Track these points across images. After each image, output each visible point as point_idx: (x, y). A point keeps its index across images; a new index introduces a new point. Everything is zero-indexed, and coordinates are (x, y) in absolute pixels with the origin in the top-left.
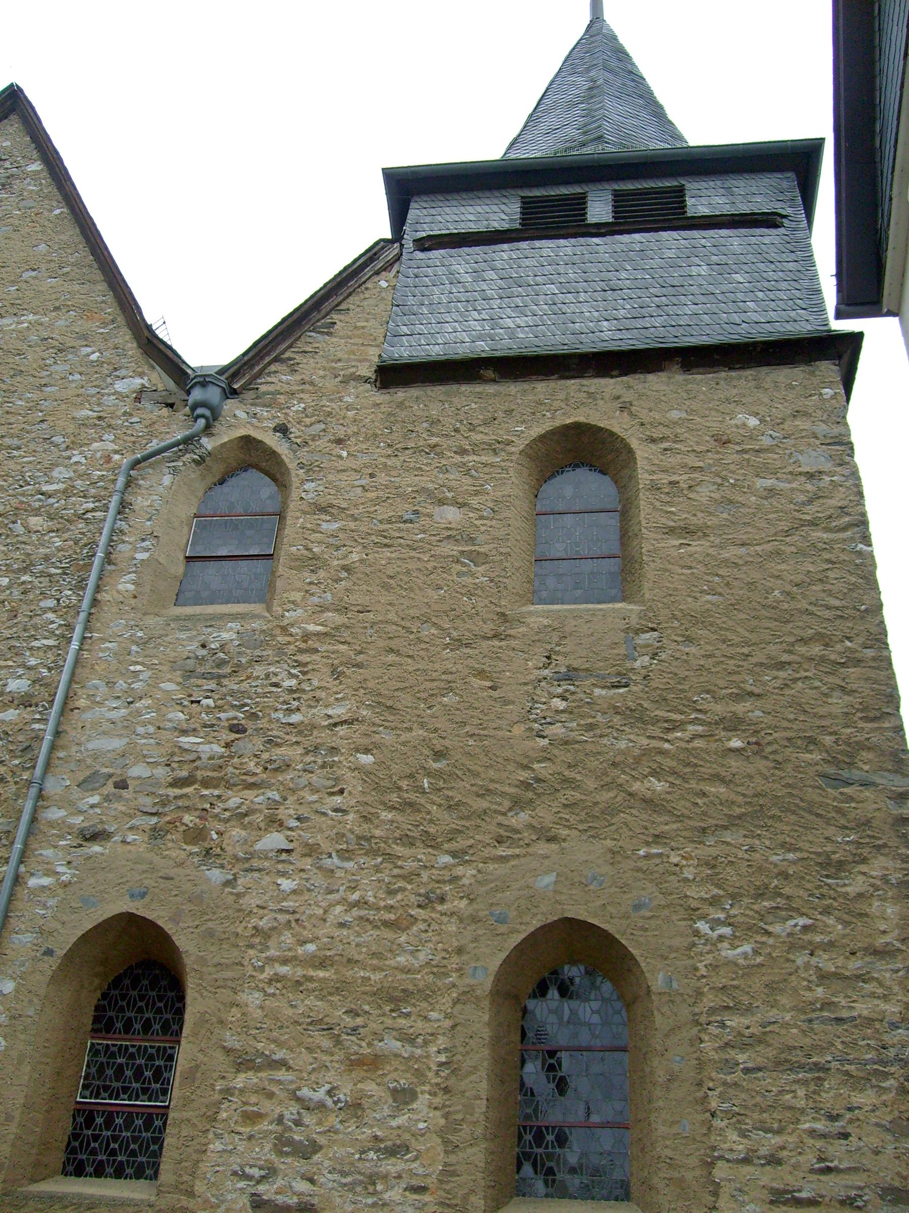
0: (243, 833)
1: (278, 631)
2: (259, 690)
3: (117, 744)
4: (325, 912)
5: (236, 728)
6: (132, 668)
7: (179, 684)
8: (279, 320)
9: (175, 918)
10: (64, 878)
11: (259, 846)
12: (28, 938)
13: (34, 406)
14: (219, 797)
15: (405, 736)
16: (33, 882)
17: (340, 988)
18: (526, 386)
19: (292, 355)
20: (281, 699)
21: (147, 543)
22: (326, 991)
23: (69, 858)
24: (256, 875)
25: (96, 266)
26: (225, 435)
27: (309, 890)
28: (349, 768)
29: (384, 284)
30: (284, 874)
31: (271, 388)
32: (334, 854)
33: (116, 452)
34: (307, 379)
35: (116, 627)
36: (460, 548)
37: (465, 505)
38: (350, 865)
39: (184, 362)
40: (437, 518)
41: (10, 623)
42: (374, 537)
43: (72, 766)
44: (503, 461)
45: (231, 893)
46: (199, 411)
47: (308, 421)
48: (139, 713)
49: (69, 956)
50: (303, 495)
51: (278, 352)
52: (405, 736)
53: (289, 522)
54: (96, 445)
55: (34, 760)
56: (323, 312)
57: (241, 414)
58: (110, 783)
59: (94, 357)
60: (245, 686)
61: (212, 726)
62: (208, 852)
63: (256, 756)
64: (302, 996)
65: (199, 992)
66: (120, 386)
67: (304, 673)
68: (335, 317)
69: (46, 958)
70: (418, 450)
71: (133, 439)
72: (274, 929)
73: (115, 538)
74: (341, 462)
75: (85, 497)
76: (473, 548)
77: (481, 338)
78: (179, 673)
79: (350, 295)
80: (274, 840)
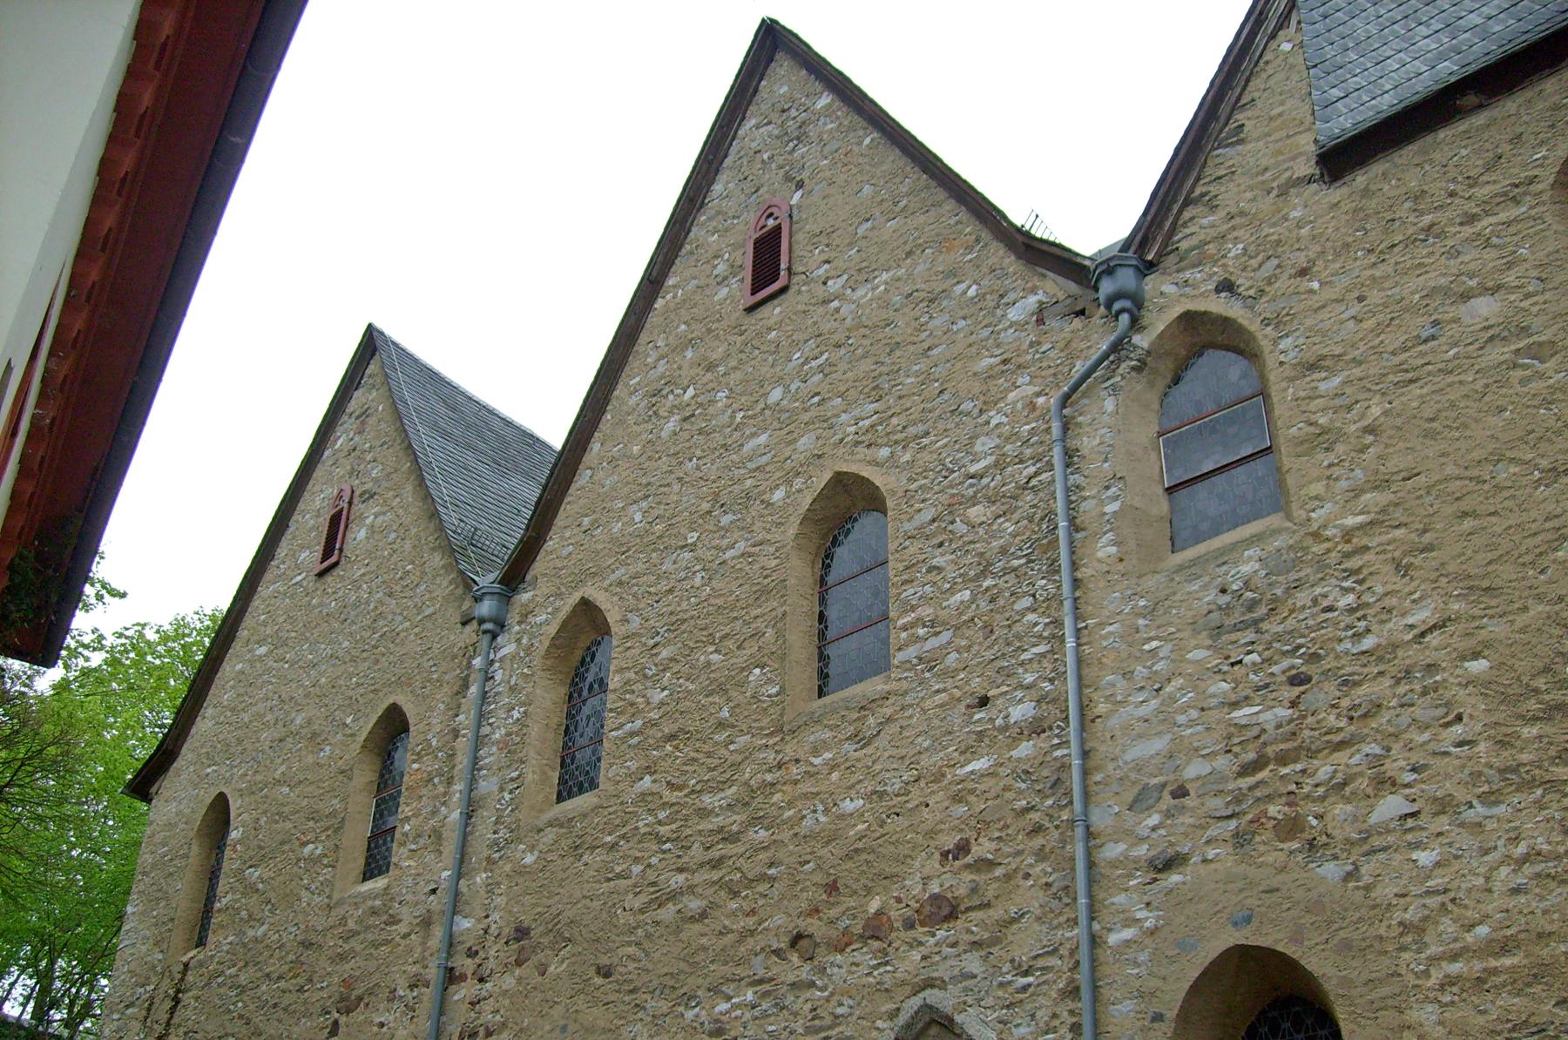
0: (1349, 808)
1: (1309, 541)
2: (1311, 622)
3: (1159, 744)
4: (1487, 879)
5: (1297, 680)
6: (1146, 647)
7: (1209, 648)
8: (1171, 153)
9: (1296, 939)
10: (1147, 924)
11: (1374, 819)
12: (1128, 1006)
13: (927, 378)
14: (1304, 771)
15: (1521, 620)
16: (1113, 939)
17: (1540, 973)
18: (1528, 94)
19: (1204, 189)
20: (1342, 625)
21: (1113, 489)
22: (1520, 983)
23: (1146, 898)
24: (1381, 856)
25: (933, 183)
26: (1159, 322)
27: (1456, 857)
28: (1460, 684)
29: (1286, 47)
30: (1418, 846)
31: (1194, 241)
32: (1475, 802)
33: (1038, 395)
34: (1233, 210)
35: (1112, 608)
36: (1513, 347)
37: (1499, 287)
38: (1501, 810)
39: (1078, 255)
40: (1467, 320)
41: (988, 642)
42: (1391, 377)
43: (1115, 787)
44: (1531, 208)
45: (1357, 888)
46: (1117, 306)
47: (1254, 263)
48: (1173, 699)
49: (1184, 1016)
50: (1282, 358)
51: (1184, 193)
52: (1521, 620)
53: (1275, 400)
54: (1012, 396)
55: (1068, 793)
56: (1222, 121)
57: (1169, 288)
58: (1166, 795)
59: (972, 292)
60: (1291, 623)
61: (1267, 686)
62: (1311, 844)
63: (1333, 706)
64: (1490, 997)
65: (1354, 1021)
66: (1013, 314)
67: (1360, 582)
68: (1240, 117)
69: (1156, 1025)
70: (1410, 242)
71: (1052, 371)
72: (1425, 919)
73: (1073, 498)
74: (1316, 298)
75: (1021, 462)
76: (1531, 340)
77: (1442, 57)
78: (1204, 634)
79: (1248, 81)
80: (1391, 806)
